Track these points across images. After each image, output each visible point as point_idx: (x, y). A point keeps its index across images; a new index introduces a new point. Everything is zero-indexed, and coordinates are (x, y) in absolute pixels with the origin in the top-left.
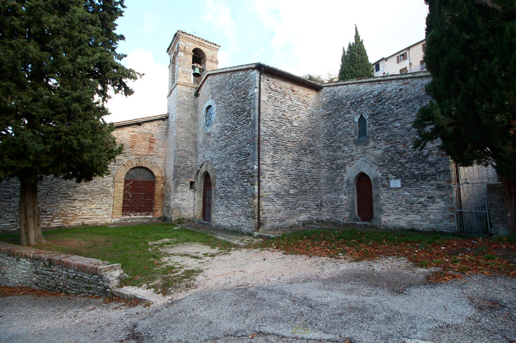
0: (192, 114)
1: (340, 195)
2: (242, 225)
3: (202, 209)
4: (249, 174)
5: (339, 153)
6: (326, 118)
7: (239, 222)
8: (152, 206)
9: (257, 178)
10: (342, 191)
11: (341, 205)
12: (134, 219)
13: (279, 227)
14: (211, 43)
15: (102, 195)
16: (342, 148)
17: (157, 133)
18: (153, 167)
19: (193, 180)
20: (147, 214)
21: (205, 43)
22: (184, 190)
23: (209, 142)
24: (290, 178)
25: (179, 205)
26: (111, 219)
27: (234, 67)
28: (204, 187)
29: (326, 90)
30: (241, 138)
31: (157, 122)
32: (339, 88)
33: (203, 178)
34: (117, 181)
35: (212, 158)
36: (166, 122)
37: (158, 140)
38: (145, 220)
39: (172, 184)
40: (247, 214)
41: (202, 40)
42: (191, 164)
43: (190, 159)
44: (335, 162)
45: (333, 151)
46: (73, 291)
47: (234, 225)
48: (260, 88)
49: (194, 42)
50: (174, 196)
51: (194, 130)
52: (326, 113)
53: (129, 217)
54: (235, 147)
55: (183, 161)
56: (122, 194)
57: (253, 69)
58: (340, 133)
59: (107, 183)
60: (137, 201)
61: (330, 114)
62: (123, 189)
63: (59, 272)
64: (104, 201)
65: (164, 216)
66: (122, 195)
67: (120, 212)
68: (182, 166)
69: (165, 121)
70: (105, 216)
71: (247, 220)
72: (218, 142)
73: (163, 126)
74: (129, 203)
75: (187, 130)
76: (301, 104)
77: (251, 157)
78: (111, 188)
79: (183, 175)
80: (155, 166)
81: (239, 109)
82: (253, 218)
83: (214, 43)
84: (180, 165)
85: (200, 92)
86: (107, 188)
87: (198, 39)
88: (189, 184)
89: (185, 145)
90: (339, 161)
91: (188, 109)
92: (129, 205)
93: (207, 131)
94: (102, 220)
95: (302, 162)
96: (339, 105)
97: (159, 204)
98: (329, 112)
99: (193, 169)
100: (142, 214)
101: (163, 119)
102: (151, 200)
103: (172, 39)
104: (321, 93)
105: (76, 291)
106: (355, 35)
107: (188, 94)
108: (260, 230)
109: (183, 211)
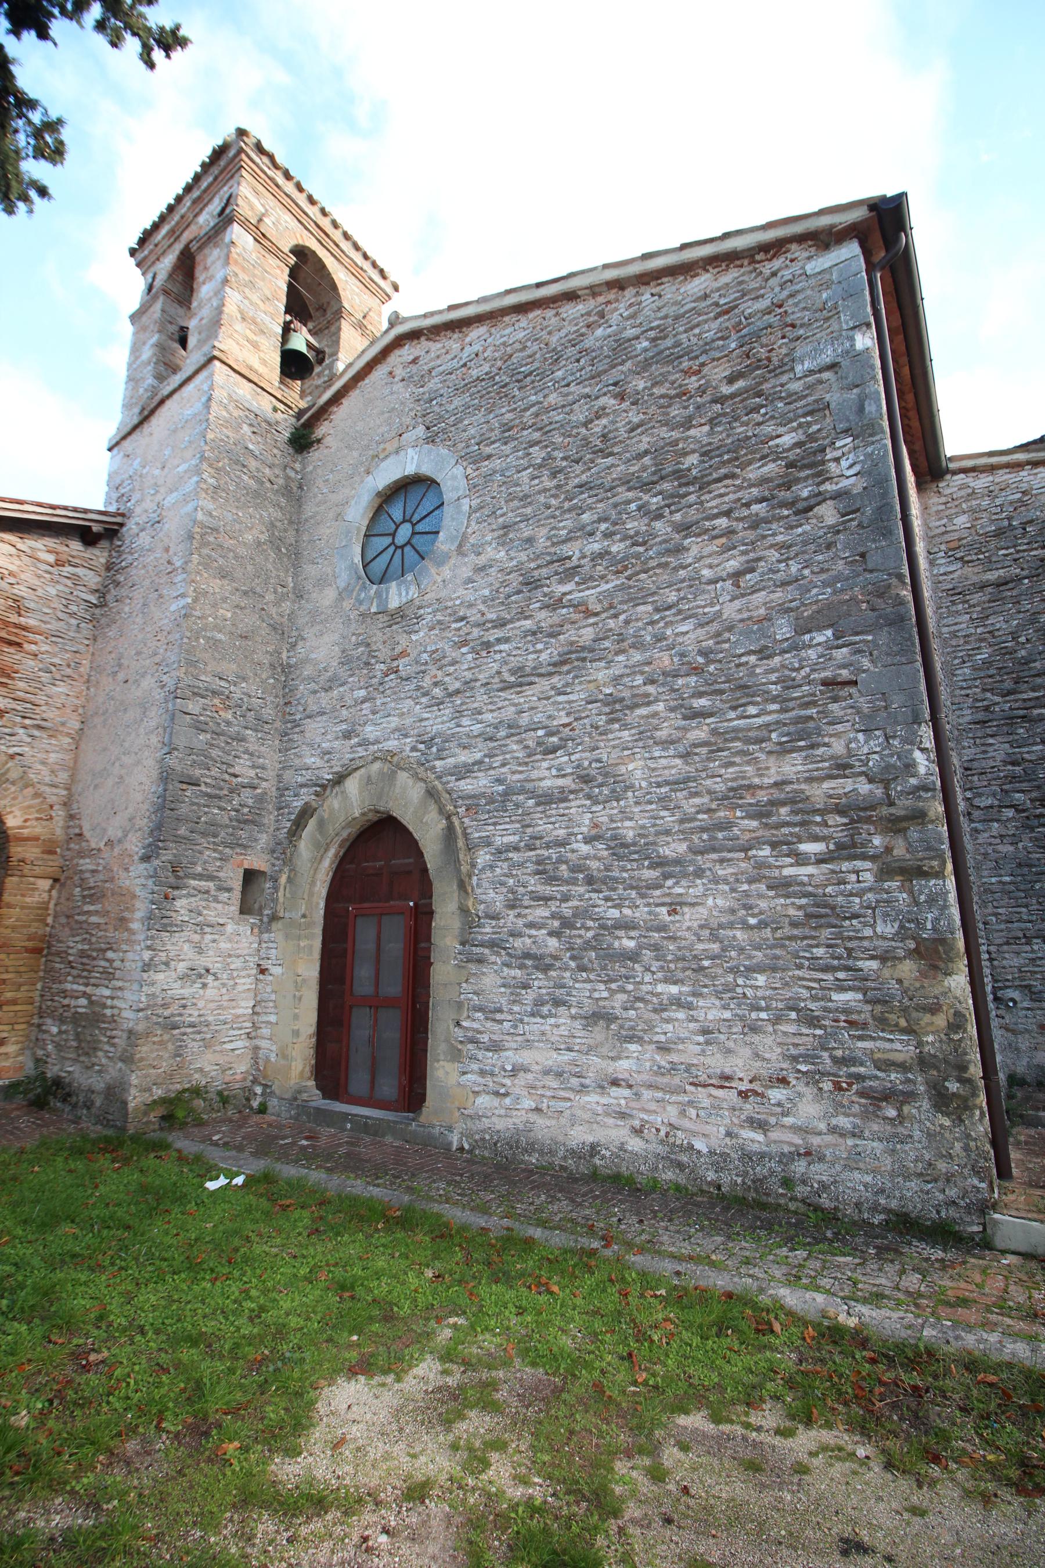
6: (976, 598)
7: (761, 1126)
17: (46, 599)
19: (257, 861)
21: (346, 246)
22: (211, 915)
23: (403, 654)
25: (174, 1009)
31: (50, 542)
36: (99, 555)
37: (48, 635)
40: (860, 1078)
42: (252, 773)
47: (700, 1145)
49: (301, 218)
50: (147, 955)
51: (277, 604)
52: (975, 579)
55: (215, 753)
68: (209, 776)
73: (79, 571)
75: (245, 593)
79: (212, 830)
81: (693, 459)
83: (381, 264)
84: (198, 772)
85: (322, 430)
88: (237, 885)
89: (230, 668)
91: (257, 494)
97: (14, 1002)
99: (261, 799)
103: (188, 178)
109: (193, 1046)
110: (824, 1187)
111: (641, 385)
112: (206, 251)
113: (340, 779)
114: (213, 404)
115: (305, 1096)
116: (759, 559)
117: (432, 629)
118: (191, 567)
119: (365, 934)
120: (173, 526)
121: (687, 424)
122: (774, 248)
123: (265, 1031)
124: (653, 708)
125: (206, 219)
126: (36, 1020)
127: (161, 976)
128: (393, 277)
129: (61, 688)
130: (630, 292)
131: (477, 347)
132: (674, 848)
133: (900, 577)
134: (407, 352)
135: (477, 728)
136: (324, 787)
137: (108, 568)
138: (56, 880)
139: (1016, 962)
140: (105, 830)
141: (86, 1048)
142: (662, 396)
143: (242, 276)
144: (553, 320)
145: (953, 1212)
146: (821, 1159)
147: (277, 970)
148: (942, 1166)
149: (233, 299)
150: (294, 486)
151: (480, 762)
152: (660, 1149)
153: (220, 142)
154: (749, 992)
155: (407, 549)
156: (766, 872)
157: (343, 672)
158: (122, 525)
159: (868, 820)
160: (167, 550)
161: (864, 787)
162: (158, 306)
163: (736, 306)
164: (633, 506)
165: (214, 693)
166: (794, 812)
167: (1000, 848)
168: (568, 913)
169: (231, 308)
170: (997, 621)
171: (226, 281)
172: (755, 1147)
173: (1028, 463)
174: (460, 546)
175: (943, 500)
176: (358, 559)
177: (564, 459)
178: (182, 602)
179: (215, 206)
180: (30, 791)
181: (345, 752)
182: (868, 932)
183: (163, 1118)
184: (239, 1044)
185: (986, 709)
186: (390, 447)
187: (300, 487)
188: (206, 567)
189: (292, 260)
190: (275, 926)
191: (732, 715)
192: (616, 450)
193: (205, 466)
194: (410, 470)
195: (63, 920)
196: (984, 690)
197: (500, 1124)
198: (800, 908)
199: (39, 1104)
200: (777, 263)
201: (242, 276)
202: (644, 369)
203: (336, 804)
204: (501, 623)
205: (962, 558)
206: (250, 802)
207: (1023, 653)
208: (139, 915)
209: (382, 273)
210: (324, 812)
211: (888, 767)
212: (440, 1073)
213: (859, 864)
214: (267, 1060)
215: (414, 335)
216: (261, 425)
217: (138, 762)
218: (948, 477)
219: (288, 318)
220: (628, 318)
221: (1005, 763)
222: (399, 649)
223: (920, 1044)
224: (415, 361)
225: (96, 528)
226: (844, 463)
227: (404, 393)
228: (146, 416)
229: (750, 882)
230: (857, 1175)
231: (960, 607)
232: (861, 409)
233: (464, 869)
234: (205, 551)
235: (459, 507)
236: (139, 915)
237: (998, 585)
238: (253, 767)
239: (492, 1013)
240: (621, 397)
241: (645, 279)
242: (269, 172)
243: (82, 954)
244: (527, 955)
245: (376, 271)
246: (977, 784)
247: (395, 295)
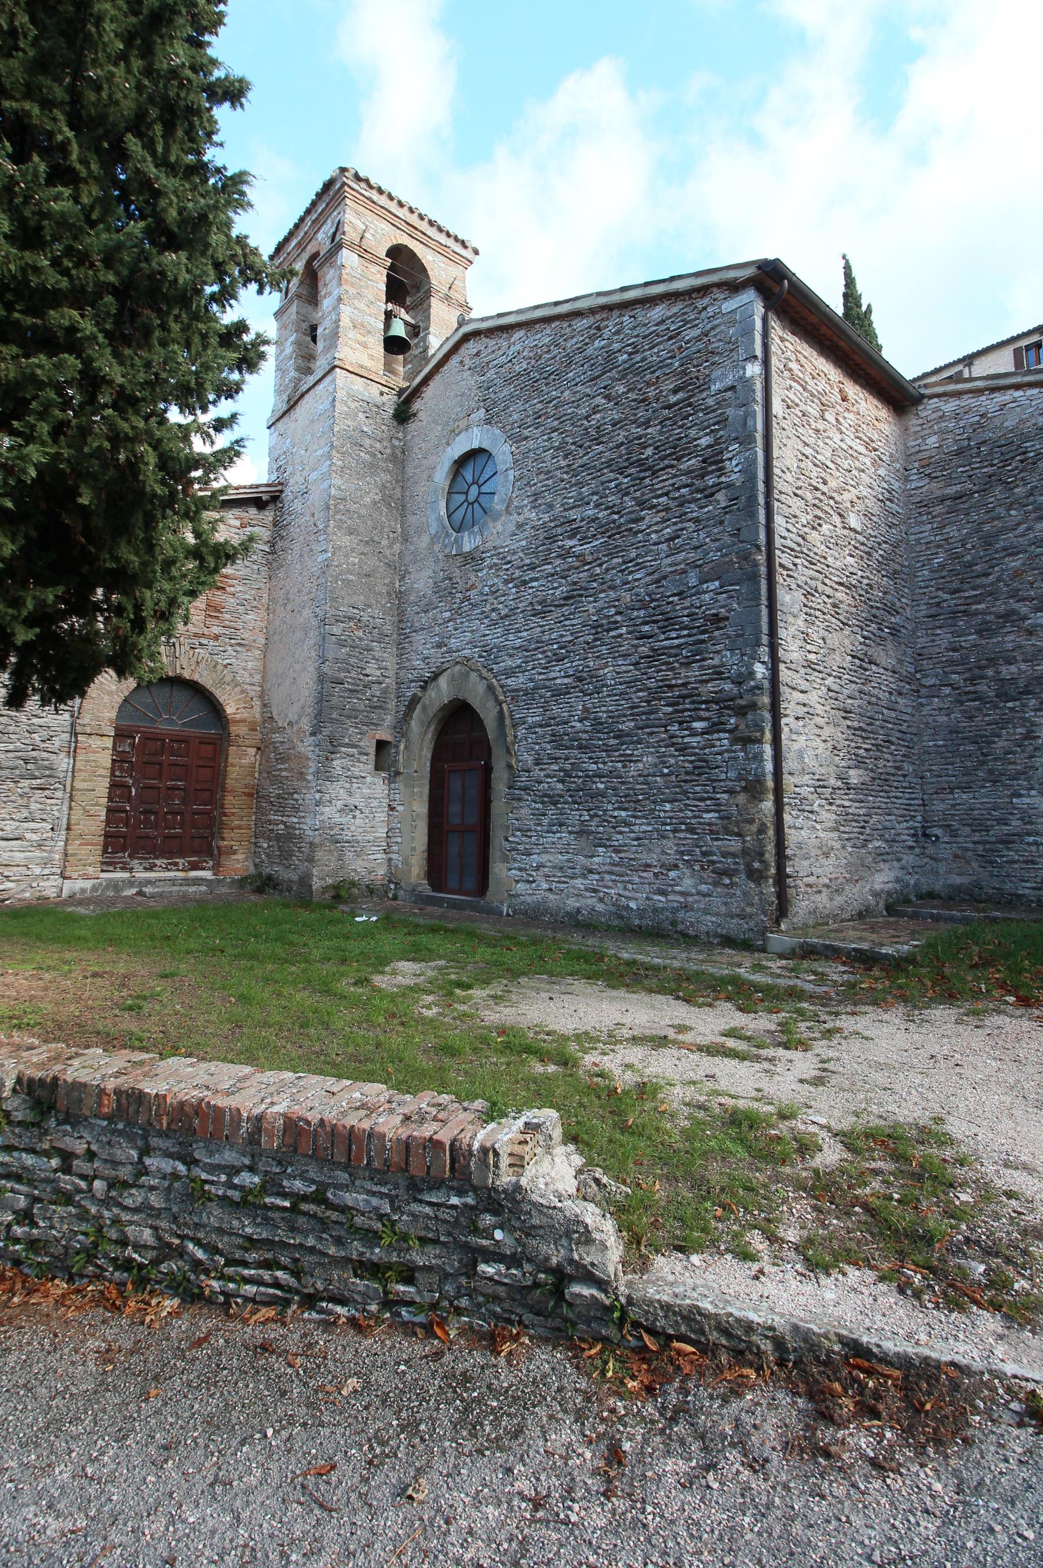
0: (384, 487)
1: (1020, 796)
2: (685, 907)
3: (425, 847)
4: (722, 701)
5: (1010, 640)
6: (938, 509)
7: (663, 893)
8: (212, 835)
9: (767, 716)
10: (1027, 779)
11: (1029, 834)
12: (149, 882)
13: (828, 916)
14: (448, 235)
15: (25, 783)
16: (1025, 618)
18: (221, 682)
19: (385, 735)
20: (195, 867)
22: (356, 771)
23: (473, 587)
24: (849, 723)
25: (336, 831)
26: (58, 881)
27: (624, 289)
28: (435, 759)
29: (937, 409)
30: (669, 560)
32: (1000, 398)
33: (433, 727)
34: (88, 730)
35: (487, 650)
36: (269, 515)
38: (192, 889)
39: (307, 747)
40: (713, 862)
41: (421, 217)
42: (378, 673)
43: (377, 655)
44: (990, 672)
45: (979, 633)
46: (247, 1280)
47: (633, 905)
48: (766, 363)
50: (318, 796)
51: (390, 547)
52: (938, 493)
53: (126, 875)
54: (627, 597)
55: (352, 661)
56: (106, 783)
57: (733, 287)
58: (1015, 563)
59: (45, 734)
60: (155, 813)
61: (958, 497)
62: (108, 764)
63: (115, 1164)
64: (34, 806)
65: (260, 875)
66: (102, 787)
67: (90, 853)
69: (267, 513)
70: (37, 871)
71: (716, 884)
72: (525, 583)
74: (128, 819)
75: (367, 543)
76: (862, 450)
77: (731, 631)
78: (62, 755)
80: (228, 679)
81: (649, 451)
82: (756, 876)
83: (460, 237)
85: (417, 405)
86: (45, 755)
87: (408, 214)
88: (372, 751)
89: (359, 600)
90: (1013, 669)
91: (372, 465)
92: (127, 825)
93: (460, 547)
94: (23, 885)
95: (874, 668)
96: (1006, 462)
97: (240, 827)
98: (954, 488)
100: (176, 864)
101: (259, 503)
102: (207, 813)
103: (307, 203)
104: (913, 423)
105: (277, 1284)
106: (843, 289)
107: (371, 409)
108: (783, 927)
109: (349, 855)
110: (692, 924)
111: (621, 389)
112: (325, 269)
113: (435, 676)
114: (337, 403)
115: (420, 889)
116: (682, 529)
117: (491, 568)
118: (330, 530)
119: (455, 785)
120: (316, 498)
121: (647, 424)
122: (703, 290)
123: (395, 848)
124: (619, 631)
125: (323, 236)
126: (253, 840)
127: (327, 809)
128: (473, 243)
129: (252, 616)
130: (616, 313)
131: (518, 347)
132: (628, 725)
133: (758, 547)
134: (471, 347)
135: (518, 642)
136: (426, 682)
137: (275, 525)
138: (259, 749)
139: (941, 806)
140: (286, 715)
141: (285, 855)
142: (634, 400)
143: (352, 291)
144: (568, 330)
145: (751, 935)
146: (692, 910)
147: (400, 808)
148: (748, 910)
149: (346, 311)
150: (398, 453)
151: (519, 667)
152: (612, 909)
153: (328, 178)
154: (662, 814)
155: (476, 505)
156: (674, 740)
157: (435, 600)
158: (281, 491)
159: (728, 708)
160: (313, 515)
161: (728, 686)
162: (294, 309)
163: (679, 334)
164: (613, 484)
165: (350, 618)
166: (691, 703)
167: (938, 718)
168: (568, 767)
169: (345, 322)
170: (951, 531)
171: (340, 299)
172: (661, 905)
173: (987, 389)
174: (508, 507)
175: (920, 421)
176: (443, 512)
177: (573, 443)
178: (325, 556)
179: (328, 228)
180: (238, 689)
181: (437, 658)
182: (723, 776)
183: (333, 897)
184: (379, 856)
185: (938, 604)
186: (463, 424)
187: (403, 452)
188: (339, 528)
189: (389, 262)
190: (398, 779)
191: (662, 637)
192: (604, 439)
193: (334, 453)
194: (475, 445)
195: (265, 775)
196: (938, 589)
197: (529, 899)
198: (691, 762)
199: (259, 891)
200: (706, 301)
201: (352, 291)
202: (624, 377)
203: (433, 694)
204: (532, 567)
205: (929, 475)
206: (378, 693)
207: (969, 557)
208: (311, 770)
209: (463, 244)
210: (426, 700)
211: (740, 674)
212: (496, 870)
213: (722, 735)
214: (397, 867)
215: (476, 334)
216: (371, 409)
217: (304, 669)
218: (925, 401)
219: (390, 306)
220: (614, 334)
221: (948, 650)
222: (470, 583)
223: (744, 842)
224: (477, 354)
225: (265, 497)
226: (734, 462)
227: (471, 380)
228: (292, 405)
229: (666, 747)
230: (709, 917)
231: (925, 517)
232: (745, 423)
233: (509, 739)
234: (338, 517)
235: (507, 476)
236: (311, 770)
237: (956, 499)
238: (379, 669)
239: (525, 831)
240: (608, 397)
241: (625, 306)
242: (366, 194)
243: (279, 796)
244: (545, 795)
245: (459, 244)
246: (926, 667)
247: (476, 259)
